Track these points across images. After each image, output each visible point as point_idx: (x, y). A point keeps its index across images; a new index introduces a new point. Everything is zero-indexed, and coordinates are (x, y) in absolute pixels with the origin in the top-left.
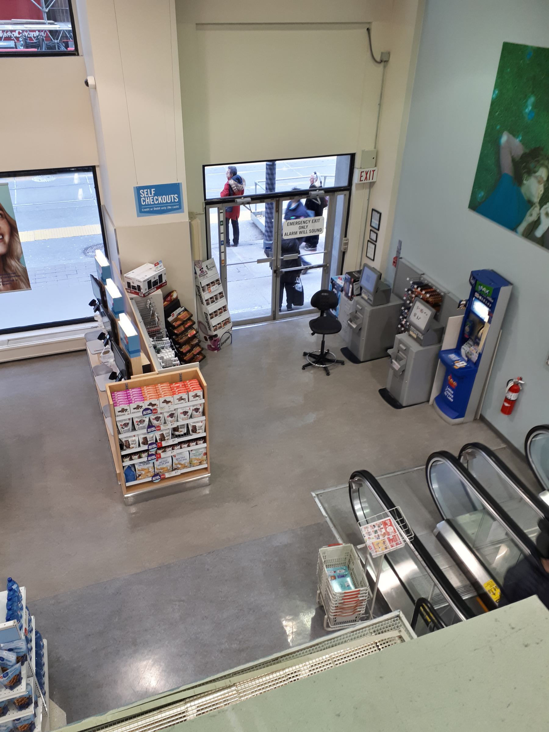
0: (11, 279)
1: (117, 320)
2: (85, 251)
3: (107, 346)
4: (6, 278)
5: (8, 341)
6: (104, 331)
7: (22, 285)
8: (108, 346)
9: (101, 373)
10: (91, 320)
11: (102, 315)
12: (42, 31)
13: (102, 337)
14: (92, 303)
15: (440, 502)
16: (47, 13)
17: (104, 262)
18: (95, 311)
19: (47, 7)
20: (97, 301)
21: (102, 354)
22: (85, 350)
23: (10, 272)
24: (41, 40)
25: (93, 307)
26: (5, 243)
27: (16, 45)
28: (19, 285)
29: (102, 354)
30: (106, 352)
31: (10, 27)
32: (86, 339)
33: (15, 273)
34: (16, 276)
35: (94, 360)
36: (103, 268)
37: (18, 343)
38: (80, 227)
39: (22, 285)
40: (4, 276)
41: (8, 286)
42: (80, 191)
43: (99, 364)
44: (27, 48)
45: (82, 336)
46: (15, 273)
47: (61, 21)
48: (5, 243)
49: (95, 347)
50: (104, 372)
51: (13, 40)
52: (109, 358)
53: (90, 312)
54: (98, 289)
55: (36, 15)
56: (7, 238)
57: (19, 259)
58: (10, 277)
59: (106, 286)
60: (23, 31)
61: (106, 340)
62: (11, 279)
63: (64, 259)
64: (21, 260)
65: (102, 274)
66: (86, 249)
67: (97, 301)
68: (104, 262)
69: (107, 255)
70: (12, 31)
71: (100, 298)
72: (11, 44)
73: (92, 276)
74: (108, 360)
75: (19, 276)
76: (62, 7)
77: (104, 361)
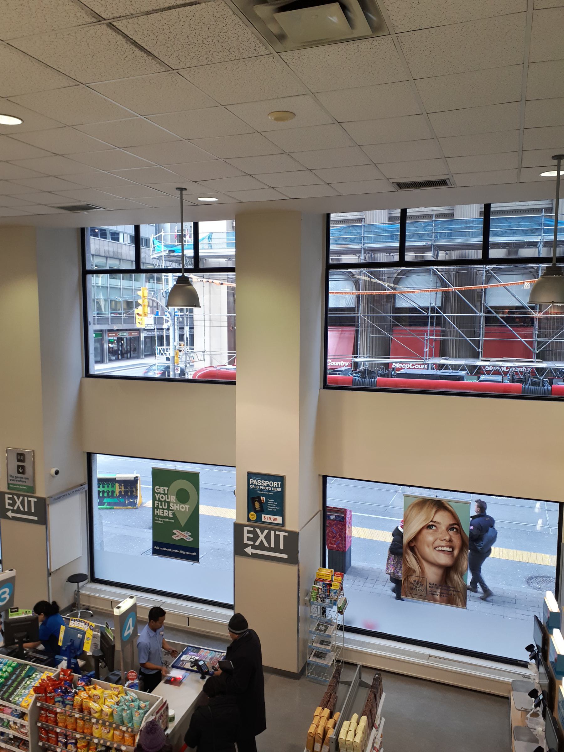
0: (450, 592)
1: (557, 681)
2: (529, 580)
3: (538, 708)
4: (444, 589)
5: (430, 656)
6: (537, 687)
7: (459, 601)
8: (540, 709)
9: (522, 738)
10: (524, 665)
11: (538, 665)
12: (529, 367)
13: (533, 694)
14: (530, 648)
15: (79, 308)
16: (537, 354)
17: (553, 606)
18: (531, 659)
19: (538, 350)
20: (536, 648)
21: (528, 716)
22: (508, 698)
23: (450, 585)
24: (527, 377)
25: (530, 653)
26: (453, 556)
27: (503, 380)
28: (456, 601)
29: (528, 716)
30: (535, 715)
31: (500, 364)
32: (512, 686)
33: (455, 588)
34: (455, 591)
35: (516, 718)
36: (552, 613)
37: (439, 662)
38: (529, 553)
39: (459, 601)
40: (443, 588)
41: (445, 598)
42: (540, 522)
43: (520, 724)
44: (513, 382)
45: (510, 680)
46: (455, 588)
47: (549, 360)
48: (453, 556)
49: (520, 701)
50: (526, 738)
51: (501, 375)
52: (538, 724)
53: (525, 656)
54: (540, 636)
55: (527, 354)
56: (456, 552)
57: (462, 576)
58: (449, 590)
59: (551, 636)
60: (511, 367)
61: (537, 700)
62: (450, 592)
63: (504, 583)
64: (464, 576)
65: (548, 618)
66: (532, 578)
67: (536, 648)
68: (553, 606)
69: (557, 597)
70: (500, 367)
71: (540, 645)
72: (499, 378)
73: (536, 617)
74: (536, 727)
75: (457, 591)
76: (552, 348)
77: (530, 725)
